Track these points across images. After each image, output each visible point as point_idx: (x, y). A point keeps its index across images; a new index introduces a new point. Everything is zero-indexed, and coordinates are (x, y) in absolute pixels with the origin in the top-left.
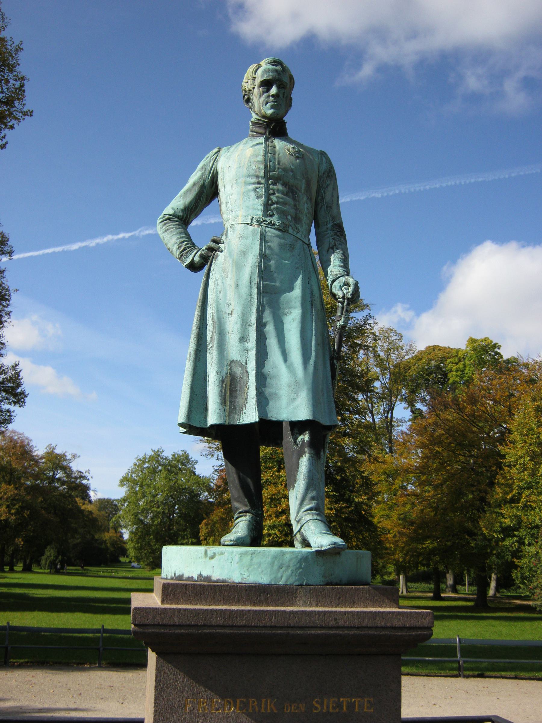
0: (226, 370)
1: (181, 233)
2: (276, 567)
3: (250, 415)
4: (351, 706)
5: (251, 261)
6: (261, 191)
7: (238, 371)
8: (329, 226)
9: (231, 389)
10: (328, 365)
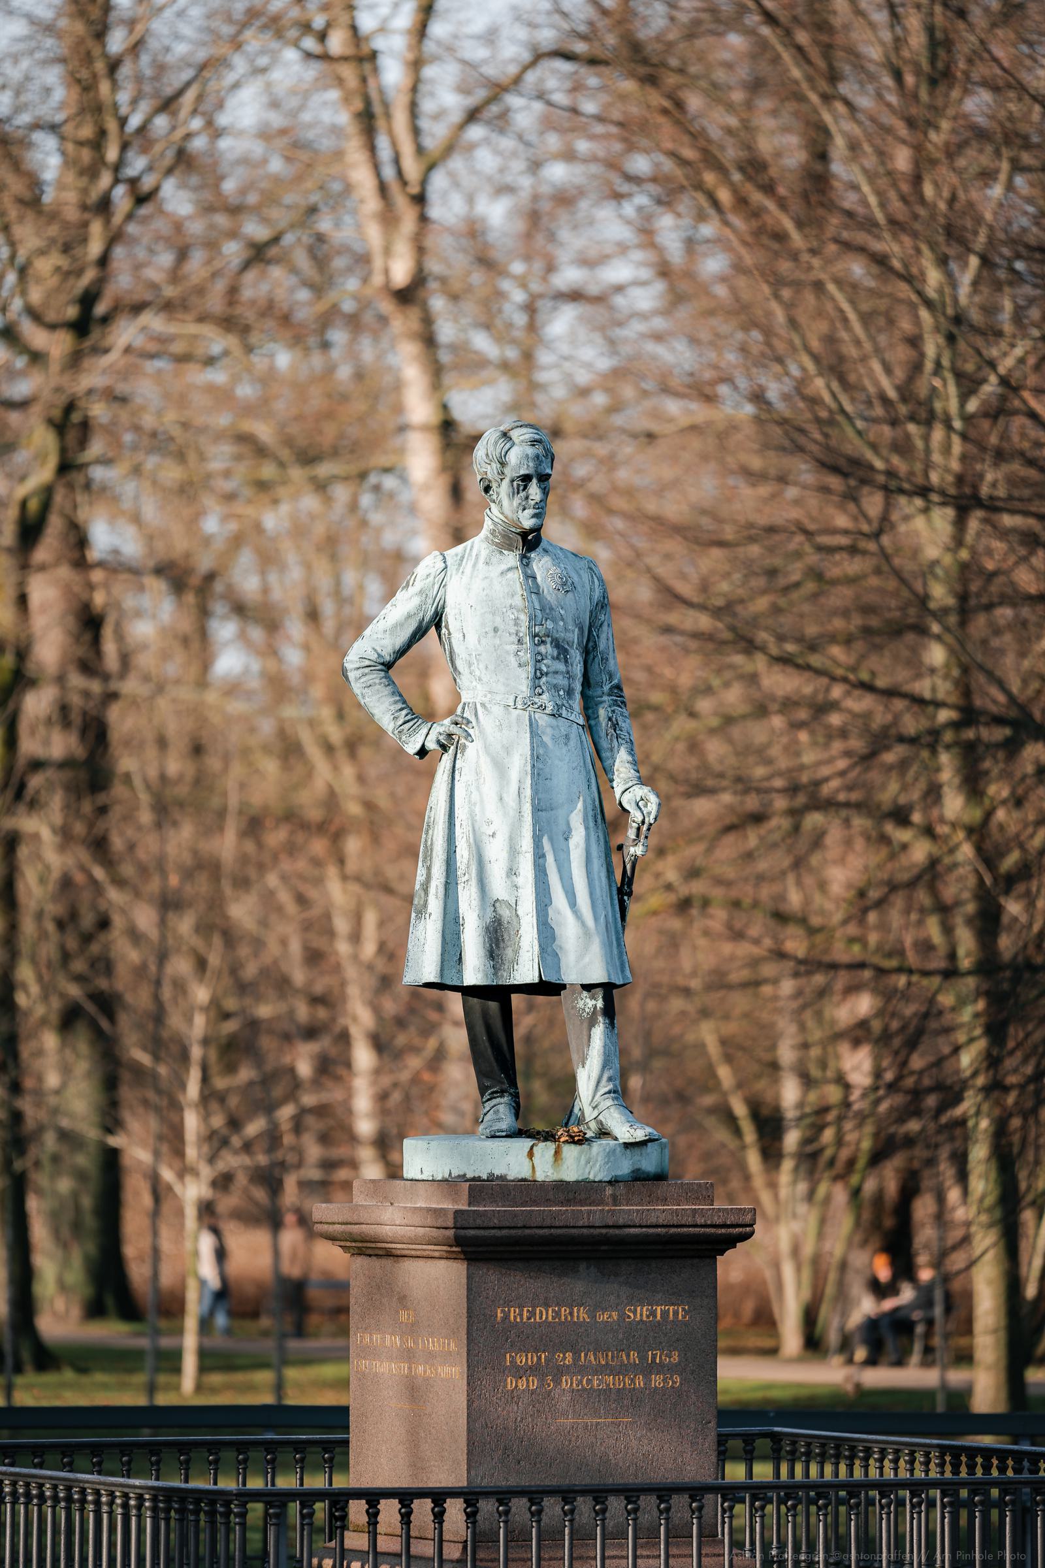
0: (489, 913)
1: (396, 702)
2: (583, 1162)
3: (526, 971)
4: (665, 1314)
5: (519, 763)
6: (527, 656)
7: (505, 913)
8: (606, 688)
9: (497, 937)
10: (616, 902)
